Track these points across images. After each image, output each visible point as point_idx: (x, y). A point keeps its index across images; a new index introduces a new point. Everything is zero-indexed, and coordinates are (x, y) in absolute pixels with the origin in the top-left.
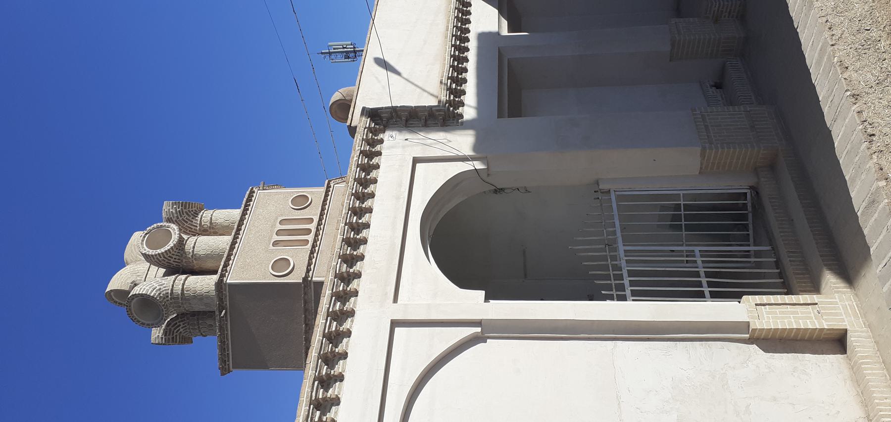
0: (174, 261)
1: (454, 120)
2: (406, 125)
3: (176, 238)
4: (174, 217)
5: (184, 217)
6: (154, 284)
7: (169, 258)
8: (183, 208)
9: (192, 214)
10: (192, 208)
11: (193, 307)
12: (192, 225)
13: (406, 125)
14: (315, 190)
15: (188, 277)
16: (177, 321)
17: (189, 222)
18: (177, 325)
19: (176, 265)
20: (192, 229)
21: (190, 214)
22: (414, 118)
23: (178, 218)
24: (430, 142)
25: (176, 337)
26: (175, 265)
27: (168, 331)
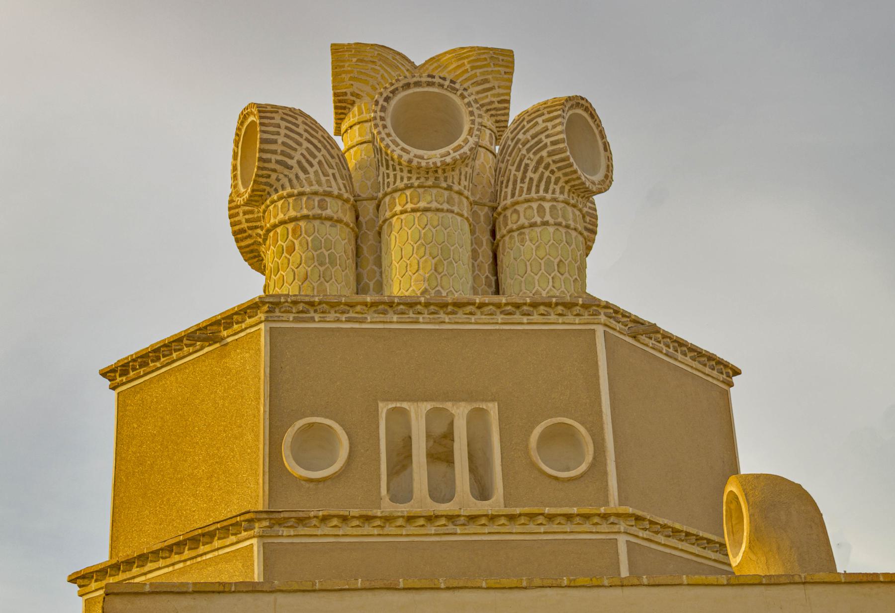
3: (431, 161)
5: (529, 159)
8: (550, 148)
9: (543, 173)
10: (559, 169)
12: (515, 182)
17: (519, 175)
20: (507, 187)
21: (541, 169)
23: (524, 145)
24: (353, 522)
25: (246, 238)
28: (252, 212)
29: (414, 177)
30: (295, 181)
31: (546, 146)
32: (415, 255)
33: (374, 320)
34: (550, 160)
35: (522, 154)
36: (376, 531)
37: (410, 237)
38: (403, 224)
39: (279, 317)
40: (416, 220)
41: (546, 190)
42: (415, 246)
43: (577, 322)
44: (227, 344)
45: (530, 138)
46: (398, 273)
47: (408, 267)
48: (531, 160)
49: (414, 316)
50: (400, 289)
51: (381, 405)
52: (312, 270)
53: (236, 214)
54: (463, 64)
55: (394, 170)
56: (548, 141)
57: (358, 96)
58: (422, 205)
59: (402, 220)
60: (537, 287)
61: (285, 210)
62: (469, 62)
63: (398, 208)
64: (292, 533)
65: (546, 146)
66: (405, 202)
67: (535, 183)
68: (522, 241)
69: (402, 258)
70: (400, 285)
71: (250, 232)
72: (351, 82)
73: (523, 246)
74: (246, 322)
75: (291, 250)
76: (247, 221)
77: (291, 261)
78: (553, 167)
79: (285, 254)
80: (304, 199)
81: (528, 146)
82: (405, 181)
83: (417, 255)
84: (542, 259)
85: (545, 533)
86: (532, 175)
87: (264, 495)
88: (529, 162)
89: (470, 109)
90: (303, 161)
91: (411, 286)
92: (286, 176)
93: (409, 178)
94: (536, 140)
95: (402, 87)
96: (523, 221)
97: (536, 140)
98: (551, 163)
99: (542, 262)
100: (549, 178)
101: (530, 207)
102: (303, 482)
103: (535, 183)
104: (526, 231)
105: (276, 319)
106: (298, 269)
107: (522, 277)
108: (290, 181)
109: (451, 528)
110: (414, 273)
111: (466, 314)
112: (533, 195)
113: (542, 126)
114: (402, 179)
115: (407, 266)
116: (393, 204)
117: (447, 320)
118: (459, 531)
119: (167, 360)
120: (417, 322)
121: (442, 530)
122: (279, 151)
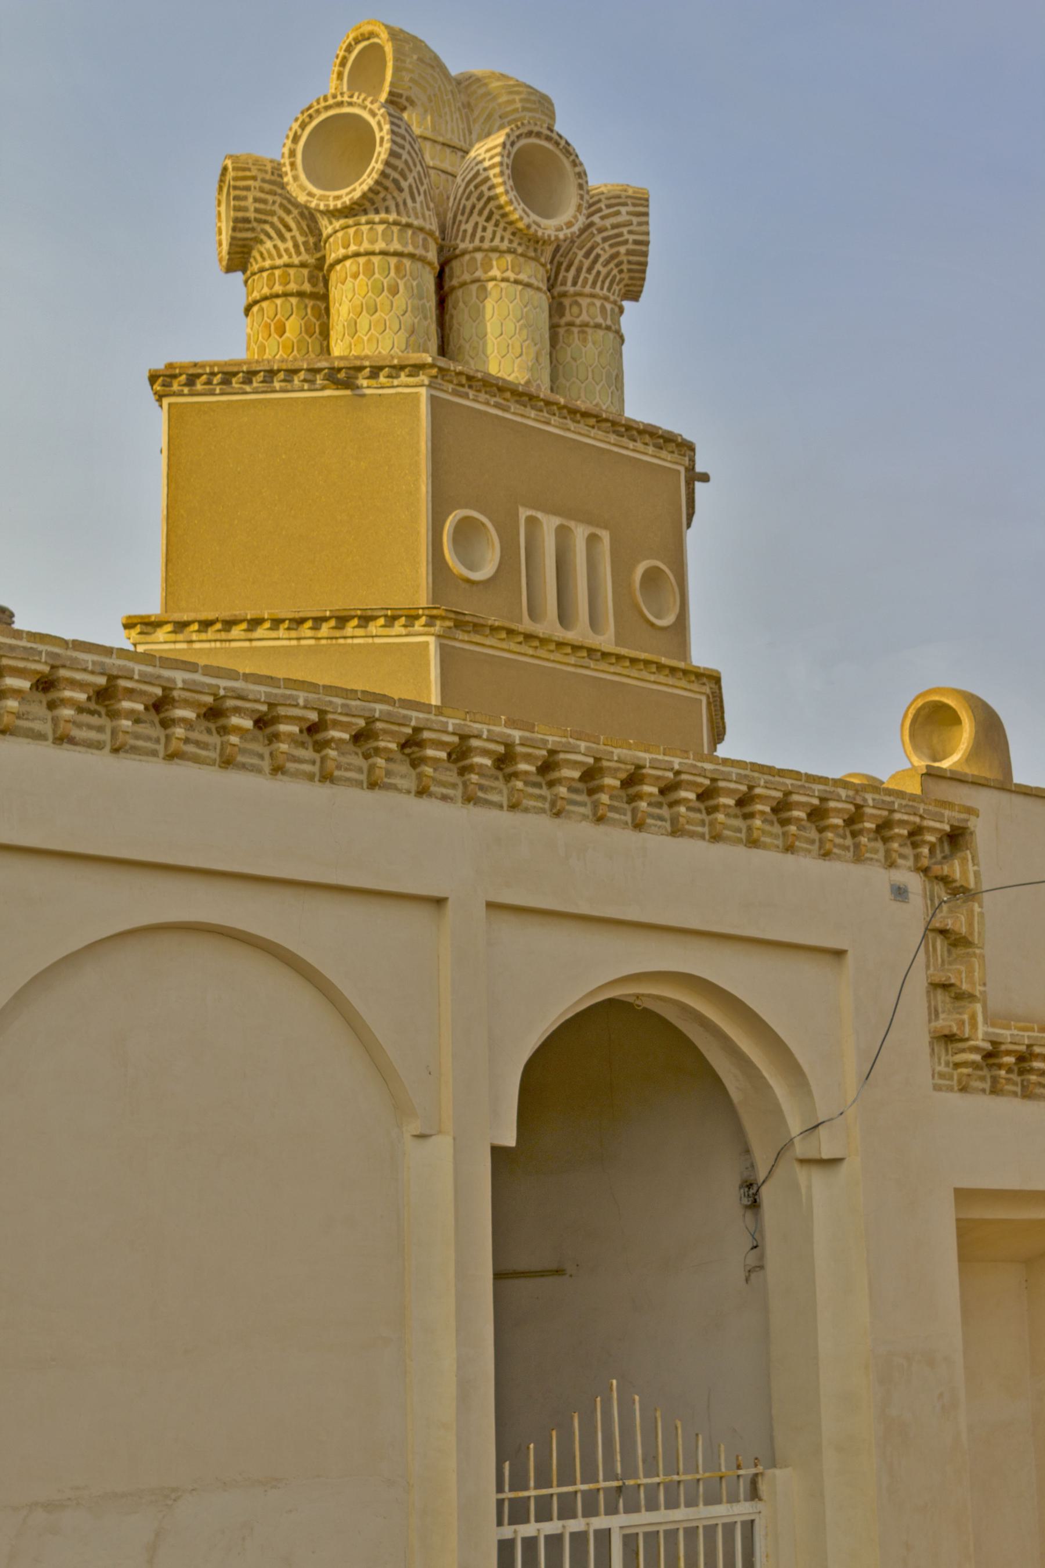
0: (477, 224)
1: (947, 1064)
2: (933, 930)
4: (602, 218)
5: (603, 249)
6: (415, 174)
7: (486, 213)
8: (631, 246)
9: (612, 269)
11: (343, 283)
12: (579, 270)
13: (933, 930)
14: (423, 489)
15: (434, 268)
16: (296, 232)
17: (587, 263)
18: (283, 230)
19: (465, 231)
20: (567, 270)
21: (612, 265)
22: (949, 951)
23: (601, 230)
25: (247, 230)
26: (463, 227)
27: (268, 208)
28: (265, 202)
29: (516, 241)
30: (402, 207)
31: (626, 242)
32: (517, 336)
33: (517, 411)
34: (625, 259)
35: (595, 242)
36: (531, 652)
37: (511, 313)
38: (503, 293)
39: (440, 384)
40: (518, 293)
41: (609, 289)
42: (518, 325)
43: (669, 459)
44: (364, 395)
45: (609, 227)
46: (496, 351)
47: (510, 347)
48: (605, 251)
49: (547, 415)
50: (370, 329)
51: (521, 510)
52: (418, 322)
53: (243, 197)
54: (513, 101)
55: (496, 225)
56: (631, 238)
57: (412, 103)
58: (523, 277)
59: (502, 289)
60: (598, 399)
61: (387, 237)
62: (521, 100)
63: (495, 272)
64: (466, 638)
65: (626, 242)
66: (506, 268)
67: (601, 279)
68: (584, 341)
69: (501, 334)
70: (500, 365)
71: (255, 224)
72: (411, 84)
73: (585, 347)
74: (400, 379)
75: (394, 291)
76: (257, 210)
77: (394, 305)
78: (625, 267)
79: (386, 293)
80: (410, 232)
81: (605, 234)
82: (506, 242)
83: (520, 336)
84: (604, 368)
85: (655, 682)
86: (601, 269)
87: (428, 588)
88: (601, 252)
89: (580, 181)
90: (414, 186)
91: (513, 371)
92: (394, 198)
93: (511, 241)
94: (616, 231)
95: (526, 134)
96: (585, 317)
97: (616, 231)
98: (625, 262)
99: (604, 371)
100: (615, 277)
101: (594, 304)
102: (460, 581)
103: (601, 279)
104: (589, 330)
105: (438, 386)
106: (405, 317)
107: (582, 383)
108: (397, 205)
109: (587, 662)
110: (502, 355)
111: (588, 426)
112: (597, 290)
113: (623, 218)
114: (502, 239)
115: (508, 346)
116: (487, 267)
117: (572, 429)
118: (592, 666)
119: (263, 387)
120: (548, 423)
121: (581, 662)
122: (400, 169)
